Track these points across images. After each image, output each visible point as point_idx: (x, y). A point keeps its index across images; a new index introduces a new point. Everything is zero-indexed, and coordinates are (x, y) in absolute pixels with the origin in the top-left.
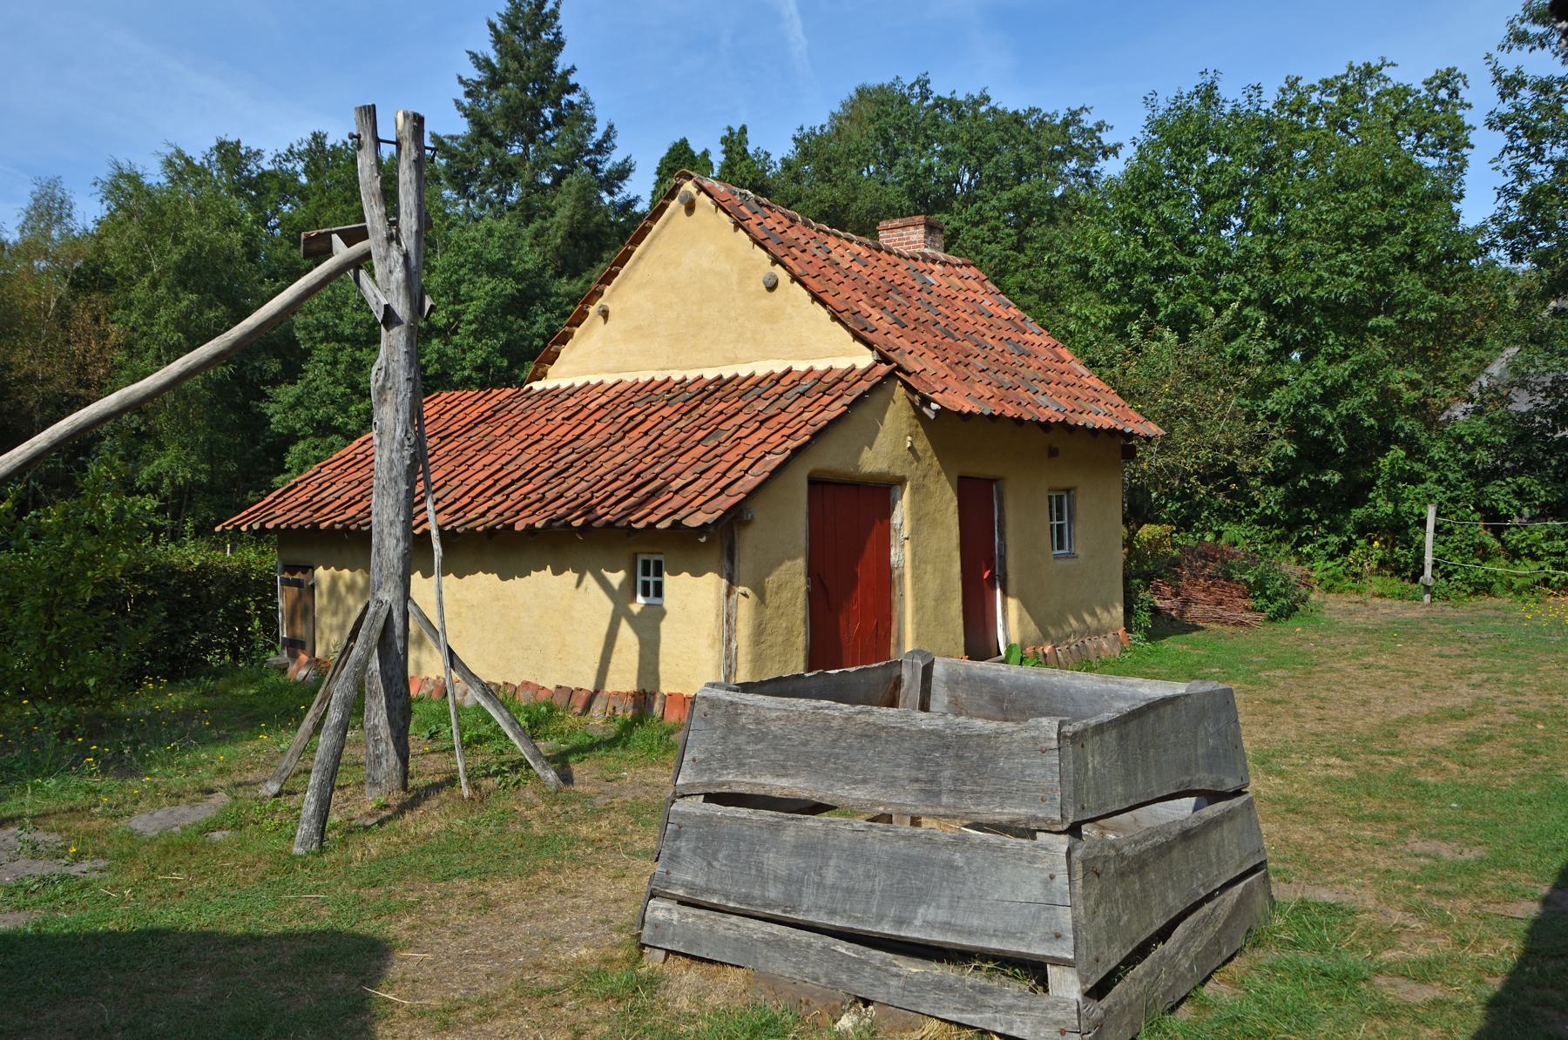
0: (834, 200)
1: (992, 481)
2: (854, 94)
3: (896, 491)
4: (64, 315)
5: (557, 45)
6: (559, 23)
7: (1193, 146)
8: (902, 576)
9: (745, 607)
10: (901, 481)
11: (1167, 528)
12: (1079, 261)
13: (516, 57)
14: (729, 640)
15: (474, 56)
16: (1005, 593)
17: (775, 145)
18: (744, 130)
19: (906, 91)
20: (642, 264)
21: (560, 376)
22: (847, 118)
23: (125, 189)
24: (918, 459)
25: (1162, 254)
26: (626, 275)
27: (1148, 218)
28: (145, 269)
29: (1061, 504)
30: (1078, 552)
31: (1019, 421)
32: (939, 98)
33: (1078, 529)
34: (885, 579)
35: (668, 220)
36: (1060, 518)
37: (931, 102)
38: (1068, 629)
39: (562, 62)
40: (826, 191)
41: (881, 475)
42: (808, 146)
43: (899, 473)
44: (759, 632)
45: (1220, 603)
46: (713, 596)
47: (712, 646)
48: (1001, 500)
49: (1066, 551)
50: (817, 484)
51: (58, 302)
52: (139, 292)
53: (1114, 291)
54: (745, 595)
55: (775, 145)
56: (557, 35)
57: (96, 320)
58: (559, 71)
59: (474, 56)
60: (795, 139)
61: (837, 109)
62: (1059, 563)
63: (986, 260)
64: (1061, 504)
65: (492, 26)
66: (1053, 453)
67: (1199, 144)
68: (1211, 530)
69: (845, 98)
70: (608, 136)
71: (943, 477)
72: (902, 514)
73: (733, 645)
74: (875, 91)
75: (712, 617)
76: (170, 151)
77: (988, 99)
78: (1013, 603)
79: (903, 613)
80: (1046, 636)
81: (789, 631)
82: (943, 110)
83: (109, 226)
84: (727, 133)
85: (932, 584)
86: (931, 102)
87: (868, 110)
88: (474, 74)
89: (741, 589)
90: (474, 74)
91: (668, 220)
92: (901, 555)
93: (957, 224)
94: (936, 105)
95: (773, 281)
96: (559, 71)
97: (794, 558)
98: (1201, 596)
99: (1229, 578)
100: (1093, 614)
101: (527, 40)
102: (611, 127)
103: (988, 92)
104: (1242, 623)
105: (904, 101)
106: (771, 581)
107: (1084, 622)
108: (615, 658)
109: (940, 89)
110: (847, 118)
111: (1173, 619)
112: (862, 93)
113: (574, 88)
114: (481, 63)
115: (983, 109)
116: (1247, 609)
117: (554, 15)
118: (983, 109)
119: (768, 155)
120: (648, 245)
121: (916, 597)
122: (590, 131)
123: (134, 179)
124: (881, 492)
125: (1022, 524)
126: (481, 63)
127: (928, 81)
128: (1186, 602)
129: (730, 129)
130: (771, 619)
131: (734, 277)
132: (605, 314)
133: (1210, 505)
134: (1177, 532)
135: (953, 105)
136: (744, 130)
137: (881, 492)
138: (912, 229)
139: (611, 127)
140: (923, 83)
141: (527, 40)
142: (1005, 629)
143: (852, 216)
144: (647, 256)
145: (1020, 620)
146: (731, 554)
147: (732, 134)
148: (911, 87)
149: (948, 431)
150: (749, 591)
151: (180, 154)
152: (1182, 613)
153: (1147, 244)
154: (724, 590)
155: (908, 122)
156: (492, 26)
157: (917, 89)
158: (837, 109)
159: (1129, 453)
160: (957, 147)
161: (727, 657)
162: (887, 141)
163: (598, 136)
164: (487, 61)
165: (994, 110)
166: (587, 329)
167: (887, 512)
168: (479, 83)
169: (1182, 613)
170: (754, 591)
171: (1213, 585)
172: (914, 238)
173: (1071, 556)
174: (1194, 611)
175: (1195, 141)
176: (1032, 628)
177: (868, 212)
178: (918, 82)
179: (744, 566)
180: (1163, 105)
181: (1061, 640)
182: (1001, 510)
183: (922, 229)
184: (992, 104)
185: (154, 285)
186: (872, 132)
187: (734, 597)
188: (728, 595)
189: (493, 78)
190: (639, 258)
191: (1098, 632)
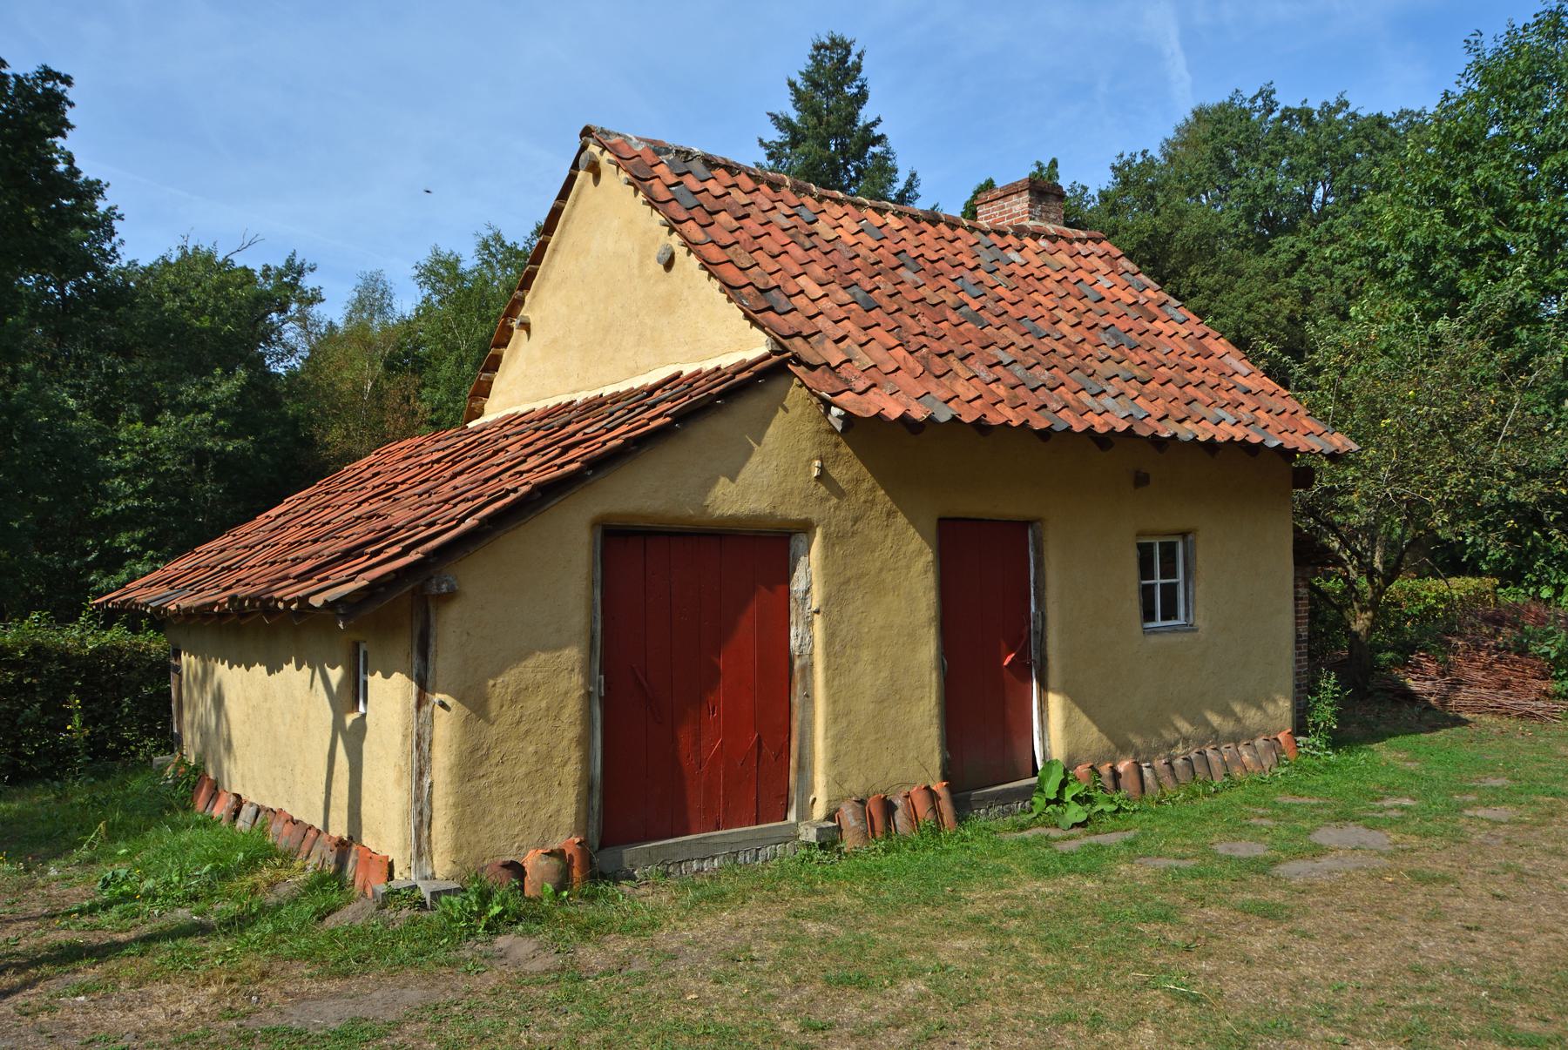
0: (1155, 228)
1: (1025, 524)
2: (1190, 116)
3: (797, 543)
4: (378, 394)
5: (861, 97)
6: (862, 75)
7: (1524, 89)
8: (808, 668)
9: (445, 726)
10: (806, 528)
11: (1489, 583)
12: (1370, 252)
13: (815, 112)
14: (421, 774)
15: (775, 117)
16: (1044, 687)
17: (1088, 174)
18: (1054, 163)
19: (1247, 105)
20: (558, 258)
21: (496, 409)
22: (1182, 144)
23: (441, 272)
24: (841, 494)
25: (1475, 231)
26: (544, 273)
27: (1460, 186)
28: (453, 348)
29: (1159, 560)
30: (1199, 623)
31: (1211, 444)
32: (1287, 109)
33: (1200, 589)
34: (779, 672)
35: (577, 196)
36: (1168, 571)
37: (1276, 114)
38: (1169, 736)
39: (866, 115)
40: (1146, 221)
41: (755, 518)
42: (1130, 176)
43: (795, 514)
44: (470, 764)
45: (1505, 685)
46: (399, 707)
47: (399, 782)
48: (1039, 551)
49: (1181, 621)
50: (616, 538)
51: (374, 386)
52: (446, 370)
53: (1407, 283)
54: (443, 705)
55: (1088, 174)
56: (861, 88)
57: (407, 399)
58: (860, 124)
59: (775, 117)
60: (1113, 168)
61: (1171, 135)
62: (1154, 639)
63: (1337, 282)
64: (1159, 560)
65: (792, 85)
66: (1141, 480)
67: (1531, 85)
68: (1548, 583)
69: (1180, 121)
70: (910, 185)
71: (901, 520)
72: (809, 575)
73: (426, 781)
74: (1215, 111)
75: (399, 738)
76: (487, 233)
77: (1346, 104)
78: (1055, 701)
79: (809, 723)
80: (1123, 748)
81: (545, 758)
82: (1292, 122)
83: (425, 311)
84: (1035, 169)
85: (868, 677)
86: (1276, 114)
87: (1205, 131)
88: (774, 135)
89: (438, 697)
90: (774, 135)
91: (577, 196)
92: (808, 637)
93: (1303, 246)
94: (1283, 117)
95: (667, 256)
96: (860, 124)
97: (559, 647)
98: (1479, 675)
99: (1523, 651)
100: (1226, 712)
101: (829, 95)
102: (914, 175)
103: (1346, 97)
104: (1531, 715)
105: (1245, 114)
106: (502, 685)
107: (1207, 724)
108: (334, 786)
109: (1287, 99)
110: (1182, 144)
111: (1429, 707)
112: (1200, 114)
113: (880, 139)
114: (782, 123)
115: (1340, 116)
116: (1546, 693)
117: (858, 69)
118: (1340, 116)
119: (1085, 189)
120: (561, 232)
121: (832, 699)
122: (891, 181)
123: (452, 265)
124: (767, 549)
125: (1081, 586)
126: (782, 123)
127: (1273, 92)
128: (1455, 685)
129: (1038, 164)
130: (500, 741)
131: (635, 258)
132: (526, 326)
133: (1547, 550)
134: (1505, 586)
135: (1305, 115)
136: (1054, 163)
137: (767, 549)
138: (1014, 198)
139: (914, 175)
140: (1267, 95)
141: (829, 95)
142: (1043, 739)
143: (1177, 246)
144: (561, 247)
145: (1068, 725)
146: (424, 648)
147: (1041, 169)
148: (1253, 100)
149: (889, 448)
150: (449, 700)
151: (498, 238)
152: (1444, 700)
153: (1453, 219)
154: (414, 699)
155: (1247, 139)
156: (792, 85)
157: (1260, 102)
158: (1171, 135)
159: (1305, 477)
160: (1301, 159)
161: (418, 799)
162: (1223, 162)
163: (899, 186)
164: (788, 121)
165: (1354, 116)
166: (514, 348)
167: (785, 574)
168: (781, 145)
169: (1444, 700)
170: (461, 699)
171: (1499, 660)
172: (1017, 209)
173: (1190, 628)
174: (1465, 695)
175: (1527, 82)
176: (1092, 736)
177: (1195, 239)
178: (1261, 93)
179: (444, 661)
180: (1489, 46)
181: (1152, 753)
182: (1040, 564)
183: (1026, 196)
184: (1351, 109)
185: (460, 362)
186: (1208, 153)
187: (426, 709)
188: (419, 706)
189: (793, 138)
190: (554, 250)
191: (1235, 739)
